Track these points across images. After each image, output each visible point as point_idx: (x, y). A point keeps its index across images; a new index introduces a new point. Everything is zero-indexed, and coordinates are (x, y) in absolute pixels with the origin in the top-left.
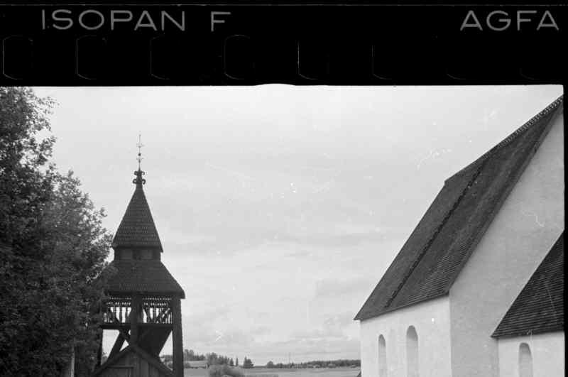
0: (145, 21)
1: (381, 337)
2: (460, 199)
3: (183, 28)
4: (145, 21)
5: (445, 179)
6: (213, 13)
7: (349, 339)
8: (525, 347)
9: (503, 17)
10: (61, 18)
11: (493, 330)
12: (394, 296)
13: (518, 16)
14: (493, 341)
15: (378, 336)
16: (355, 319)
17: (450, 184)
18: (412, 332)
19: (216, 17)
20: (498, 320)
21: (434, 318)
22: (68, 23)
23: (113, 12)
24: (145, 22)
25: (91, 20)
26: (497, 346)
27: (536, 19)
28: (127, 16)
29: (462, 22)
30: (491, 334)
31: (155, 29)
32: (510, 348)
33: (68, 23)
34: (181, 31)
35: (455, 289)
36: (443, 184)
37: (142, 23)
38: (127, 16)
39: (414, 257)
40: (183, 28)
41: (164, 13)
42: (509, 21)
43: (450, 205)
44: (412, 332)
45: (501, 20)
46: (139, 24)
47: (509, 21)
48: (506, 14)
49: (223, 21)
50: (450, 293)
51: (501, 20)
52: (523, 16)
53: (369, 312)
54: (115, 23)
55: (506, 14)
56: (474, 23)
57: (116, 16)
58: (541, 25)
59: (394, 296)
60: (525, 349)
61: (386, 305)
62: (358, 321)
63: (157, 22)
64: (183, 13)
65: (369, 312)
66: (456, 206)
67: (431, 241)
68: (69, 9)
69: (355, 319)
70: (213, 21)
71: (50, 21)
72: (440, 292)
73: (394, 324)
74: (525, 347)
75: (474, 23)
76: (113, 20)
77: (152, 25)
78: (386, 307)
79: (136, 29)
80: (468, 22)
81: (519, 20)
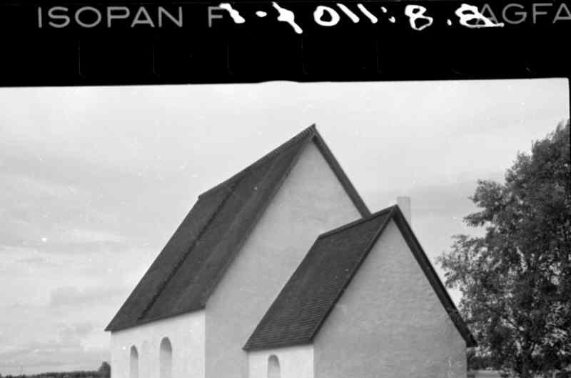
0: (142, 17)
1: (134, 349)
2: (214, 215)
3: (180, 23)
4: (142, 17)
5: (201, 192)
6: (535, 5)
7: (86, 350)
8: (274, 359)
9: (519, 10)
10: (58, 17)
11: (245, 342)
12: (149, 308)
13: (534, 9)
14: (243, 353)
15: (161, 339)
16: (107, 329)
17: (204, 199)
18: (166, 344)
19: (113, 13)
20: (58, 364)
21: (189, 331)
22: (64, 21)
23: (110, 9)
24: (142, 18)
25: (88, 17)
26: (248, 359)
27: (552, 12)
28: (123, 12)
29: (555, 14)
30: (243, 345)
31: (153, 25)
32: (260, 361)
33: (64, 21)
34: (177, 26)
35: (211, 302)
36: (196, 200)
37: (560, 15)
38: (123, 12)
39: (169, 270)
40: (180, 23)
41: (161, 10)
42: (525, 14)
43: (204, 221)
44: (166, 344)
45: (517, 13)
46: (136, 21)
47: (525, 14)
48: (522, 7)
49: (545, 13)
50: (207, 306)
51: (517, 13)
52: (538, 9)
53: (120, 323)
54: (213, 20)
55: (522, 7)
56: (145, 19)
57: (113, 13)
58: (557, 18)
59: (149, 308)
60: (273, 362)
61: (140, 316)
62: (109, 333)
63: (155, 20)
64: (180, 9)
65: (120, 323)
66: (210, 221)
67: (187, 254)
68: (523, 5)
69: (107, 329)
70: (211, 17)
71: (46, 19)
72: (196, 306)
73: (147, 336)
74: (274, 359)
75: (145, 19)
76: (110, 17)
77: (149, 21)
78: (140, 318)
79: (554, 22)
80: (140, 19)
81: (535, 13)
